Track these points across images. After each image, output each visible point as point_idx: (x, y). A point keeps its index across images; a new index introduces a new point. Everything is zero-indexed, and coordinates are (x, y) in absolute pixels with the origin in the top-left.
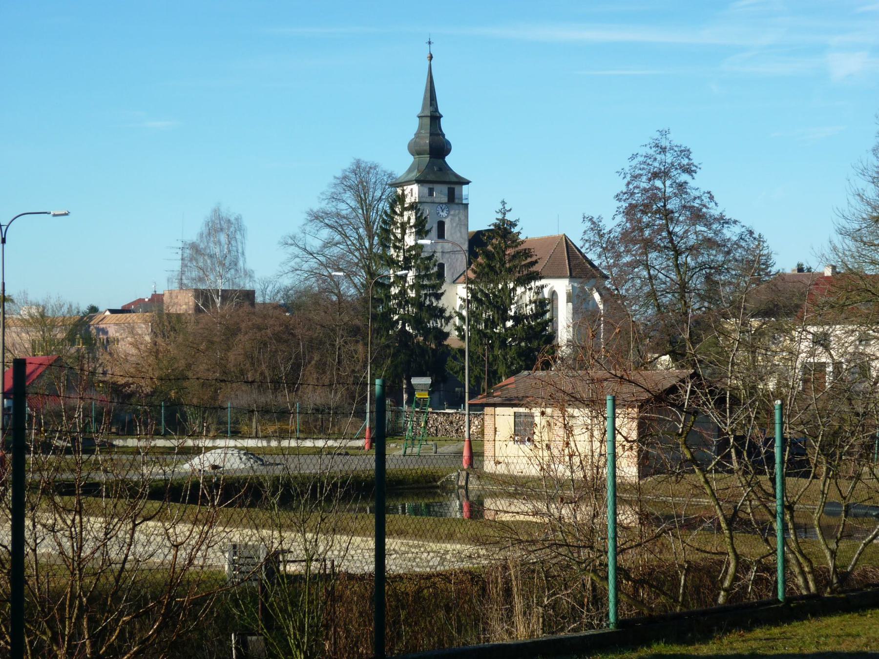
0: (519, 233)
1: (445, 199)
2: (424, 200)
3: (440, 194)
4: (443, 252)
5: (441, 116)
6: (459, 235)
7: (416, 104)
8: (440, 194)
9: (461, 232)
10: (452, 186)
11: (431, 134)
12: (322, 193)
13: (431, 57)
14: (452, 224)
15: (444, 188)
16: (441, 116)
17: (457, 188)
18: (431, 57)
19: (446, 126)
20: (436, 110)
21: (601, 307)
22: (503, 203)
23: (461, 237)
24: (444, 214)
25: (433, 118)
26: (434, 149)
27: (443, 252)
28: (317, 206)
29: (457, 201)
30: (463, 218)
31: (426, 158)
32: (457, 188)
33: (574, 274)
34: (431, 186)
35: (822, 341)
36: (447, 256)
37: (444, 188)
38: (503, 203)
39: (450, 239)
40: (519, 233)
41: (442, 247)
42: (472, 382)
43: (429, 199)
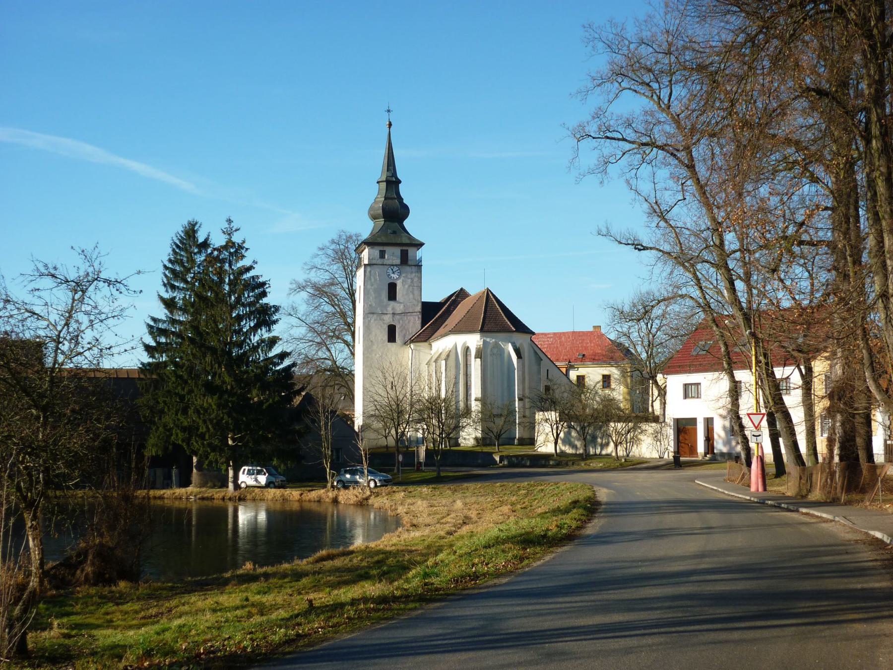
1: (398, 261)
2: (374, 262)
3: (393, 255)
4: (394, 314)
5: (400, 182)
7: (378, 170)
8: (393, 255)
11: (386, 198)
12: (305, 264)
13: (390, 125)
14: (404, 285)
15: (397, 251)
16: (400, 182)
17: (411, 251)
18: (390, 125)
19: (403, 190)
20: (394, 174)
22: (230, 221)
24: (395, 276)
25: (392, 183)
26: (393, 211)
27: (394, 314)
28: (301, 277)
29: (410, 263)
30: (416, 280)
31: (381, 222)
32: (411, 251)
33: (485, 328)
34: (381, 248)
35: (690, 391)
36: (398, 317)
37: (397, 251)
38: (230, 221)
41: (393, 309)
42: (701, 488)
43: (380, 261)
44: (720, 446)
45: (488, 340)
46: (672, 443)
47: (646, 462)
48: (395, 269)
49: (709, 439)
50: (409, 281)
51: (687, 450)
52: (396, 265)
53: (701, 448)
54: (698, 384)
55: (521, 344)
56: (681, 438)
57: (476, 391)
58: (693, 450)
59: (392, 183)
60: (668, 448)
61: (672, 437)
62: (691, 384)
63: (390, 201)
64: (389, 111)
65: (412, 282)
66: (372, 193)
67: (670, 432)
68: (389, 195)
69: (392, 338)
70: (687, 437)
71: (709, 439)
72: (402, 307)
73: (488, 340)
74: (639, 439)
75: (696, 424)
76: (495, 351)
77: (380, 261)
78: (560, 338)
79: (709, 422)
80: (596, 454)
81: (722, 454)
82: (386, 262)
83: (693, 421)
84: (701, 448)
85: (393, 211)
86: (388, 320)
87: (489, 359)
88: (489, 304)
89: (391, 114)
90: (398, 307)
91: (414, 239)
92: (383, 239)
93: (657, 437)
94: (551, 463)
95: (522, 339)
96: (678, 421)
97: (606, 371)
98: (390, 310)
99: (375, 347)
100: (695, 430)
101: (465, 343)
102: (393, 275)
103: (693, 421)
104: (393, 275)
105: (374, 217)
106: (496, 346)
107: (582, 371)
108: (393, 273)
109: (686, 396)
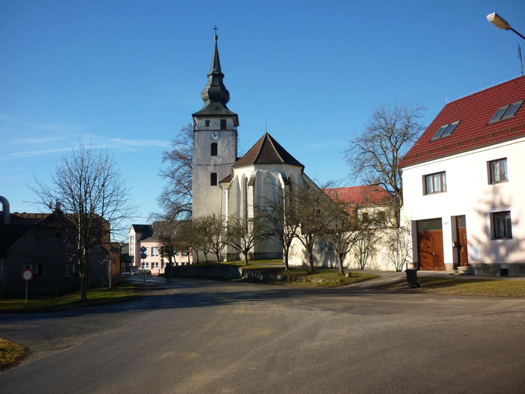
0: (348, 265)
1: (219, 128)
2: (202, 129)
3: (215, 123)
4: (215, 165)
6: (228, 152)
8: (215, 123)
9: (229, 151)
10: (223, 119)
11: (212, 86)
14: (222, 145)
15: (218, 121)
18: (217, 38)
19: (225, 81)
21: (283, 186)
23: (230, 153)
24: (216, 138)
25: (218, 76)
26: (218, 95)
27: (215, 165)
28: (170, 148)
29: (227, 128)
31: (209, 102)
34: (206, 119)
36: (218, 167)
37: (218, 121)
39: (221, 156)
40: (348, 265)
41: (215, 161)
43: (206, 128)
44: (476, 253)
45: (261, 171)
46: (411, 253)
47: (376, 277)
48: (216, 133)
49: (460, 244)
50: (227, 141)
51: (430, 260)
52: (217, 130)
53: (448, 258)
54: (443, 173)
55: (292, 174)
56: (422, 245)
57: (251, 214)
58: (438, 261)
59: (218, 76)
60: (407, 258)
61: (411, 245)
62: (433, 175)
63: (214, 88)
64: (216, 29)
65: (228, 142)
66: (205, 83)
67: (408, 239)
68: (214, 84)
69: (214, 182)
70: (429, 244)
71: (460, 244)
72: (221, 160)
73: (261, 171)
74: (374, 249)
75: (440, 227)
76: (268, 180)
77: (206, 128)
78: (353, 190)
79: (459, 222)
80: (332, 267)
81: (484, 267)
82: (210, 128)
83: (437, 222)
84: (448, 258)
85: (218, 95)
86: (211, 169)
87: (262, 186)
88: (266, 144)
89: (217, 30)
90: (218, 160)
91: (230, 112)
92: (208, 113)
93: (394, 245)
94: (279, 277)
95: (291, 171)
96: (417, 224)
97: (382, 209)
98: (212, 163)
99: (201, 189)
100: (440, 235)
101: (244, 175)
102: (214, 138)
103: (437, 222)
104: (214, 138)
105: (205, 100)
106: (269, 175)
107: (364, 210)
108: (215, 136)
109: (426, 191)
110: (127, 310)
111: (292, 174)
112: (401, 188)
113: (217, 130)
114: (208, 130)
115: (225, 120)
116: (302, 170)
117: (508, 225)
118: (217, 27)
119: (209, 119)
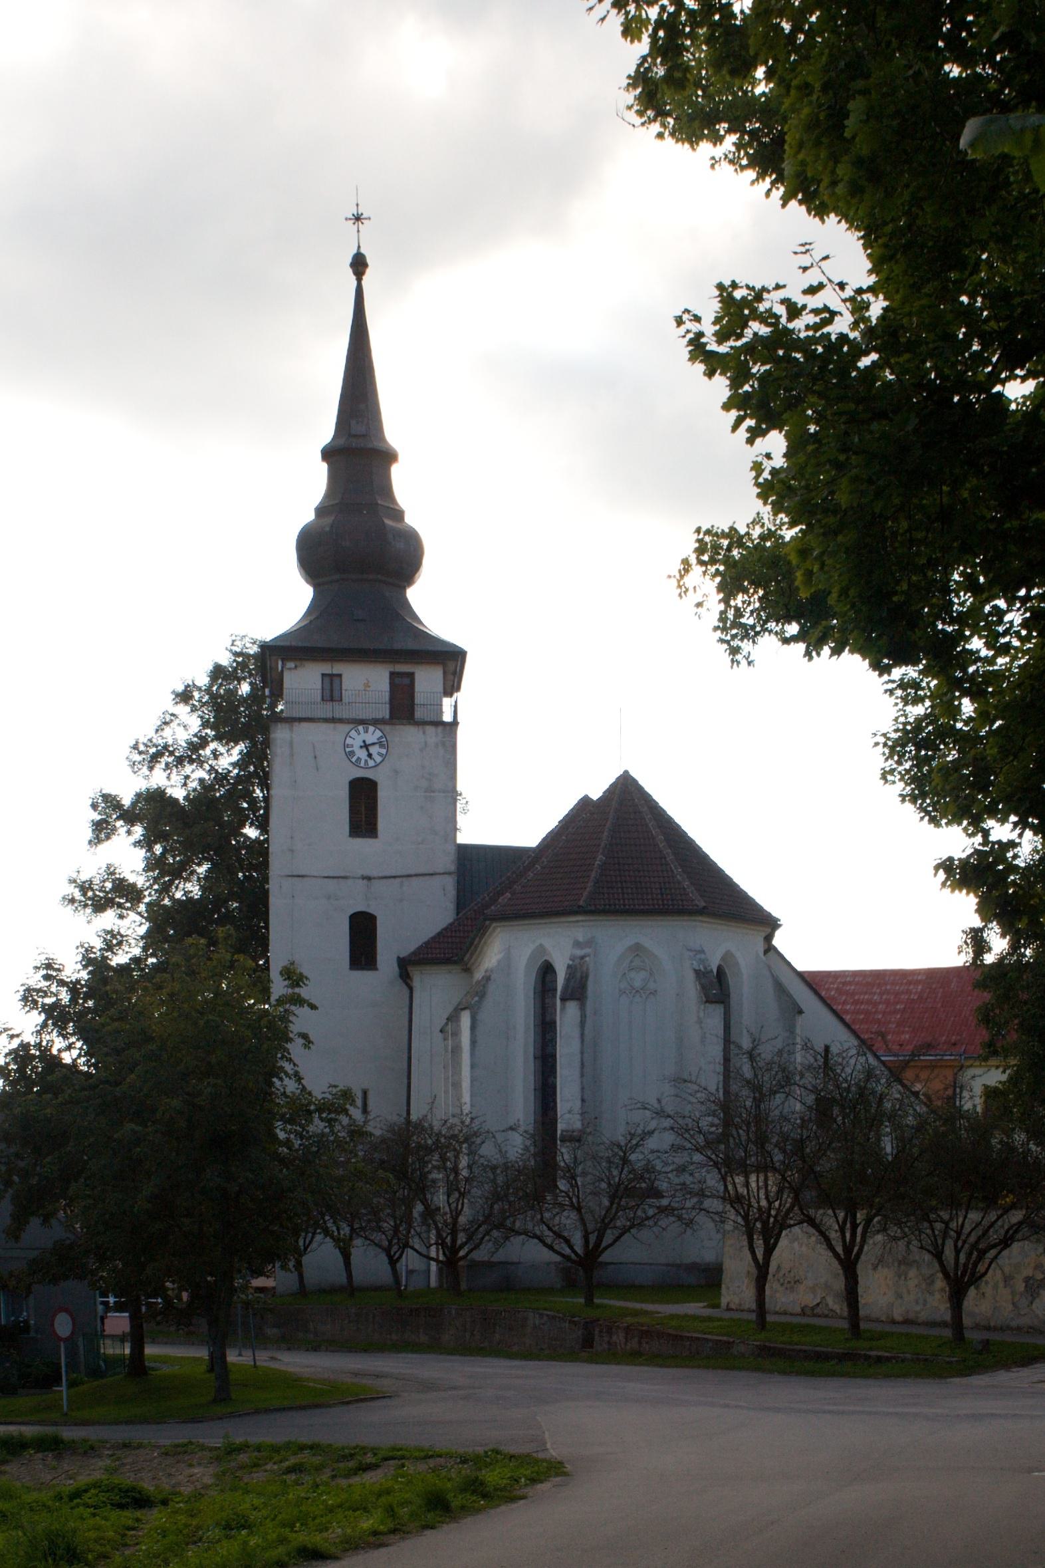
1: (385, 712)
18: (359, 265)
25: (358, 452)
29: (419, 714)
34: (326, 668)
43: (326, 710)
59: (358, 452)
64: (358, 218)
77: (326, 710)
82: (340, 711)
110: (771, 1372)
111: (728, 956)
112: (455, 723)
113: (376, 722)
114: (333, 720)
115: (411, 676)
116: (769, 938)
117: (718, 1285)
118: (365, 211)
119: (338, 668)
